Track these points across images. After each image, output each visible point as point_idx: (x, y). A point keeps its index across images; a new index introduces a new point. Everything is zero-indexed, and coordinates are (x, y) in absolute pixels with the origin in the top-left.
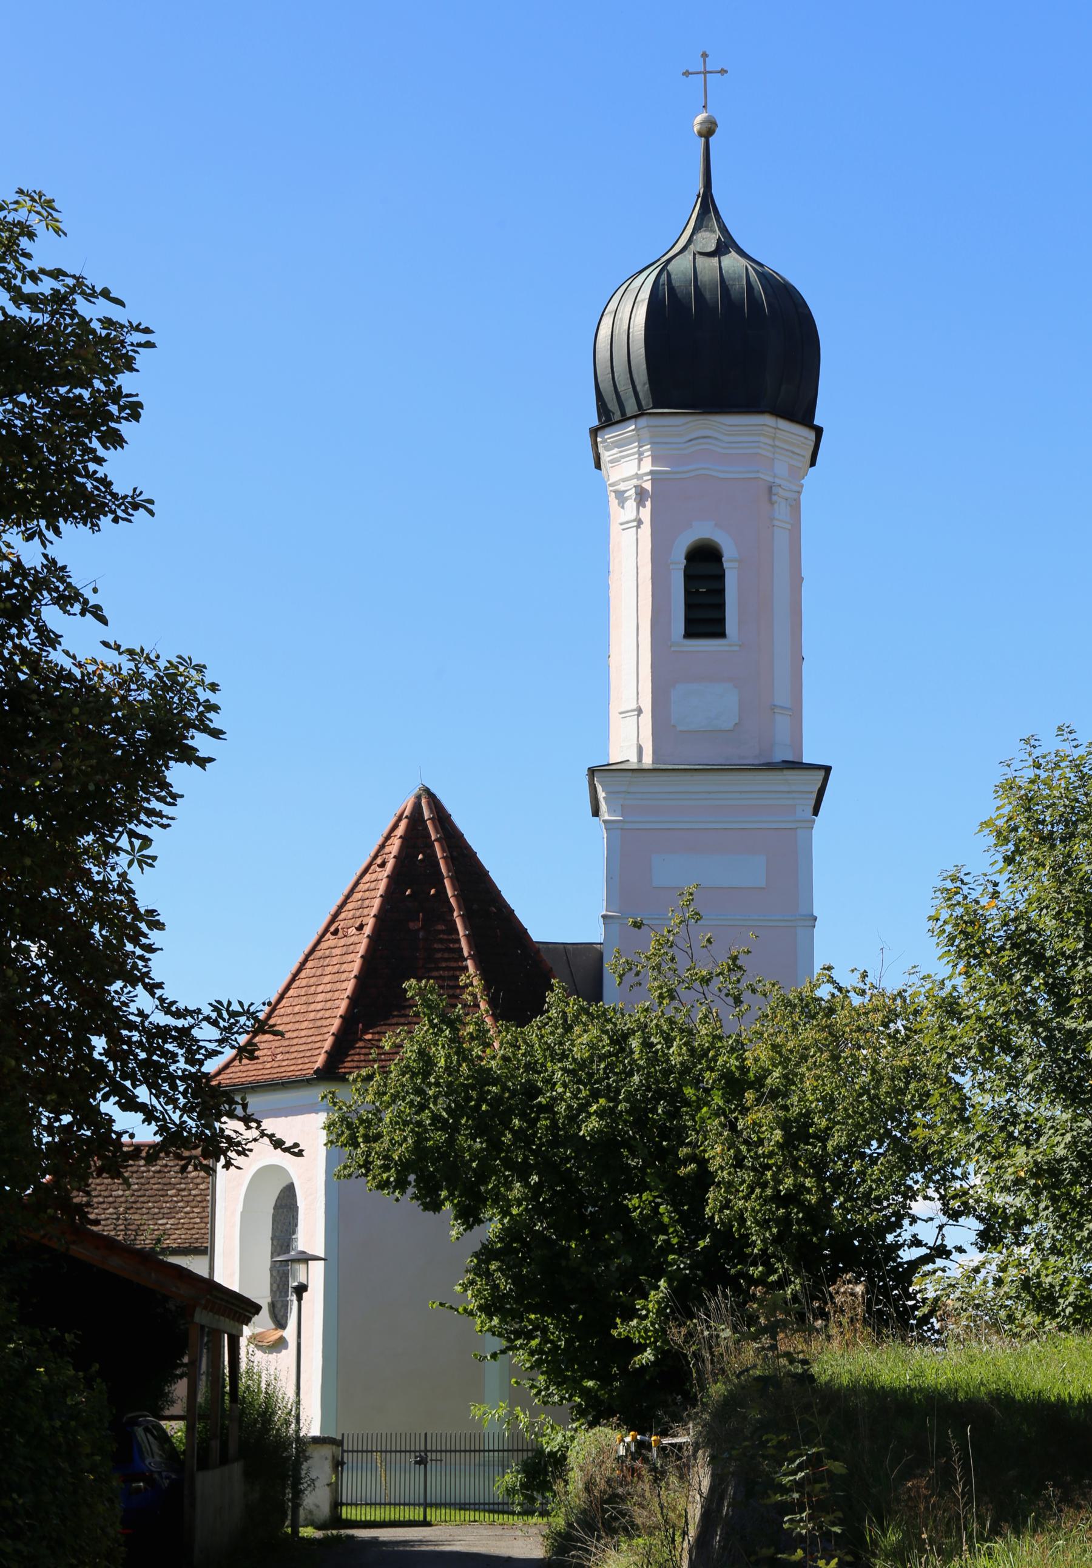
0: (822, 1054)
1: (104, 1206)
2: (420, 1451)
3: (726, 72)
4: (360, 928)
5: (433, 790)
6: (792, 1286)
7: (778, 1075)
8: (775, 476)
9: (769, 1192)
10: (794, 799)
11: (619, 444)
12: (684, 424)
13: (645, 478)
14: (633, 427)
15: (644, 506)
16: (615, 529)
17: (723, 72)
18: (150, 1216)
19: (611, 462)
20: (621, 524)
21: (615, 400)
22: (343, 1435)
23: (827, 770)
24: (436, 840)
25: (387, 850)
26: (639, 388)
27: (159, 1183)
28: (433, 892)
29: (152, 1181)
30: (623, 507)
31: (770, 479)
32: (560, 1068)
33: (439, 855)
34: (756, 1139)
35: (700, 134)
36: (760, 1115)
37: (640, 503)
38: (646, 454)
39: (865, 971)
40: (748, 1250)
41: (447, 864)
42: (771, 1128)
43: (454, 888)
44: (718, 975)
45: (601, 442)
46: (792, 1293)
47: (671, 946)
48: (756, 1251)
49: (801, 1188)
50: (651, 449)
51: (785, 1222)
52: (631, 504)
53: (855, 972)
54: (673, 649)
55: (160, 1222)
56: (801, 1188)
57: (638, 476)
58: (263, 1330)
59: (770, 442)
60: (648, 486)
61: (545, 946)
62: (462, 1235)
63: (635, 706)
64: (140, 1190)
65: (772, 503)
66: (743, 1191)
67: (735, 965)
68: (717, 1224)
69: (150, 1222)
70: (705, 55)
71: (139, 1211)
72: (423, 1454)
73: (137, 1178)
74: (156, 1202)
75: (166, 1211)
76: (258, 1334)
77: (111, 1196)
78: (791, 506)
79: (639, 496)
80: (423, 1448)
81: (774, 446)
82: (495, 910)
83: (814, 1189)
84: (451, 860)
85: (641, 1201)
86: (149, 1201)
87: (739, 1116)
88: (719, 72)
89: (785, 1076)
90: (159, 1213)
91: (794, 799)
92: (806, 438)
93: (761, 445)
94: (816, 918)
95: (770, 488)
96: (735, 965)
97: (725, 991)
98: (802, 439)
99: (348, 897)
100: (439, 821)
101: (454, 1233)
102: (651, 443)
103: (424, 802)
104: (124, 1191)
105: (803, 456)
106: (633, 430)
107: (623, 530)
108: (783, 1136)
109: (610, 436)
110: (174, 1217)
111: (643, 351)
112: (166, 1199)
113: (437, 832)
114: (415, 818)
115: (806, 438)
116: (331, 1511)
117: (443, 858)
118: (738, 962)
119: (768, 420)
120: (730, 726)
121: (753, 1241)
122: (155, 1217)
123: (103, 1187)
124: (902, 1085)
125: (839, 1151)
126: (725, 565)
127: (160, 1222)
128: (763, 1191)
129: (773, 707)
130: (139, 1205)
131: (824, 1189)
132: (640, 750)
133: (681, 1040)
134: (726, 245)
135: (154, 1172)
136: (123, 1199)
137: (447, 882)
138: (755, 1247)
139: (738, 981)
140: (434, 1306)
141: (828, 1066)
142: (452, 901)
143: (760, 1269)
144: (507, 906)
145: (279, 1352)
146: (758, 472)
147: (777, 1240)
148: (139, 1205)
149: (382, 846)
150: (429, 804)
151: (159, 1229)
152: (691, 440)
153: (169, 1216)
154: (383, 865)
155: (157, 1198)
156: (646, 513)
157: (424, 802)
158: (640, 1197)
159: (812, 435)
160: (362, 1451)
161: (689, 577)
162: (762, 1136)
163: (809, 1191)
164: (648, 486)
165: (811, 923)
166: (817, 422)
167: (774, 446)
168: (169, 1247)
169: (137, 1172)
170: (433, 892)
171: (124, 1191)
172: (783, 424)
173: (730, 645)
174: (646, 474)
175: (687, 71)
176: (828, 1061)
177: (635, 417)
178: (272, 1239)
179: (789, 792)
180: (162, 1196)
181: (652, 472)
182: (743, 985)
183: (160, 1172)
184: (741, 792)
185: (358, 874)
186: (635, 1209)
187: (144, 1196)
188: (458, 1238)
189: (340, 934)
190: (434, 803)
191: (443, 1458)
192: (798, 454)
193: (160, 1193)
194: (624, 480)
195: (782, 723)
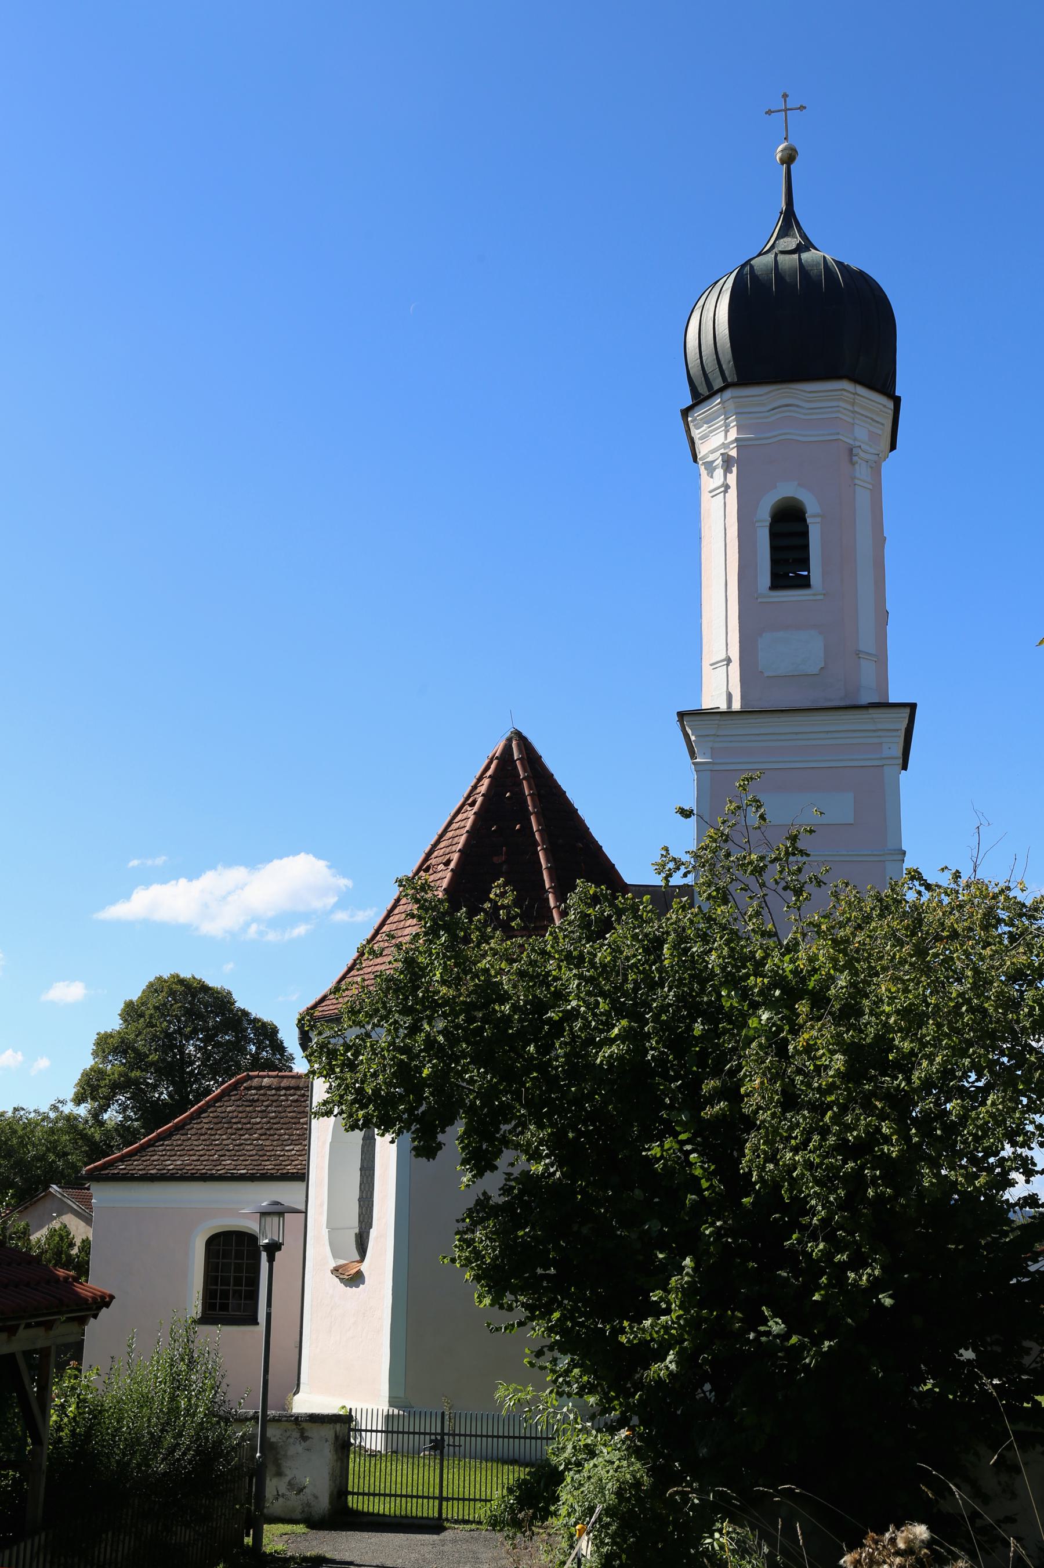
0: (902, 947)
1: (241, 1132)
2: (436, 1434)
3: (805, 108)
4: (447, 863)
5: (525, 733)
6: (869, 1270)
7: (844, 984)
8: (855, 439)
9: (832, 1140)
10: (880, 737)
11: (708, 421)
12: (767, 394)
13: (731, 446)
14: (719, 400)
15: (731, 472)
16: (705, 496)
17: (802, 108)
18: (280, 1142)
19: (701, 438)
20: (710, 492)
21: (704, 383)
22: (351, 1409)
23: (913, 707)
24: (524, 778)
25: (478, 791)
26: (724, 367)
27: (294, 1112)
28: (518, 827)
29: (288, 1110)
30: (712, 477)
31: (851, 442)
32: (575, 975)
33: (527, 793)
34: (812, 1068)
35: (782, 162)
36: (814, 1033)
37: (727, 470)
38: (732, 425)
39: (957, 871)
40: (805, 1220)
41: (533, 800)
42: (829, 1051)
43: (539, 823)
44: (772, 861)
45: (692, 421)
46: (868, 1280)
47: (726, 841)
48: (815, 1221)
49: (874, 1137)
50: (736, 420)
51: (856, 1182)
52: (719, 473)
53: (946, 871)
54: (759, 600)
55: (287, 1148)
56: (874, 1137)
57: (724, 446)
58: (346, 1262)
59: (849, 407)
60: (734, 453)
61: (645, 889)
62: (474, 1182)
63: (724, 656)
64: (276, 1117)
65: (853, 463)
66: (796, 1138)
67: (795, 849)
68: (756, 1183)
69: (279, 1148)
70: (785, 96)
71: (271, 1138)
72: (439, 1437)
73: (276, 1107)
74: (288, 1129)
75: (295, 1137)
76: (341, 1266)
77: (249, 1123)
78: (871, 467)
79: (725, 464)
80: (439, 1431)
81: (854, 412)
82: (581, 845)
83: (894, 1138)
84: (538, 797)
85: (663, 1150)
86: (282, 1129)
87: (790, 1037)
88: (799, 108)
89: (853, 985)
90: (289, 1139)
91: (880, 737)
92: (885, 406)
93: (841, 410)
94: (904, 853)
95: (851, 450)
96: (795, 849)
97: (783, 884)
98: (881, 407)
99: (441, 836)
100: (529, 762)
101: (465, 1179)
102: (736, 414)
103: (514, 743)
104: (262, 1118)
105: (883, 424)
106: (719, 404)
107: (712, 497)
108: (846, 1061)
109: (699, 413)
110: (301, 1144)
111: (727, 332)
112: (298, 1126)
113: (525, 771)
114: (505, 759)
115: (885, 406)
116: (331, 1503)
117: (530, 795)
118: (800, 845)
119: (846, 385)
120: (816, 671)
121: (812, 1207)
122: (285, 1143)
123: (244, 1115)
124: (702, 1395)
125: (927, 1084)
126: (809, 521)
127: (287, 1148)
128: (824, 1139)
129: (858, 653)
130: (272, 1132)
131: (908, 1138)
132: (730, 697)
133: (721, 938)
134: (806, 245)
135: (292, 1101)
136: (258, 1126)
137: (533, 818)
138: (814, 1215)
139: (800, 870)
140: (446, 1261)
141: (911, 964)
142: (537, 836)
143: (821, 1246)
144: (595, 843)
145: (357, 1287)
146: (838, 434)
147: (843, 1205)
148: (272, 1132)
149: (475, 787)
150: (518, 745)
151: (284, 1155)
152: (773, 409)
153: (297, 1142)
154: (473, 804)
155: (289, 1126)
156: (732, 479)
157: (514, 743)
158: (661, 1146)
159: (890, 405)
160: (409, 1433)
161: (773, 535)
162: (819, 1063)
163: (887, 1140)
164: (734, 453)
165: (900, 857)
166: (897, 394)
167: (854, 412)
168: (288, 1173)
169: (277, 1100)
170: (518, 827)
171: (262, 1118)
172: (861, 390)
173: (814, 595)
174: (732, 442)
175: (770, 110)
176: (912, 956)
177: (721, 390)
178: (361, 1169)
179: (874, 731)
180: (295, 1124)
181: (737, 440)
182: (804, 877)
183: (297, 1101)
184: (827, 732)
185: (452, 814)
186: (658, 1160)
187: (279, 1123)
188: (468, 1186)
189: (431, 871)
190: (525, 745)
191: (462, 1443)
192: (878, 422)
193: (293, 1121)
194: (713, 452)
195: (867, 671)
